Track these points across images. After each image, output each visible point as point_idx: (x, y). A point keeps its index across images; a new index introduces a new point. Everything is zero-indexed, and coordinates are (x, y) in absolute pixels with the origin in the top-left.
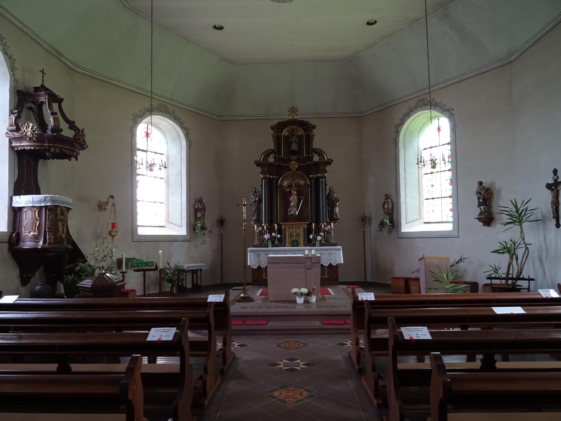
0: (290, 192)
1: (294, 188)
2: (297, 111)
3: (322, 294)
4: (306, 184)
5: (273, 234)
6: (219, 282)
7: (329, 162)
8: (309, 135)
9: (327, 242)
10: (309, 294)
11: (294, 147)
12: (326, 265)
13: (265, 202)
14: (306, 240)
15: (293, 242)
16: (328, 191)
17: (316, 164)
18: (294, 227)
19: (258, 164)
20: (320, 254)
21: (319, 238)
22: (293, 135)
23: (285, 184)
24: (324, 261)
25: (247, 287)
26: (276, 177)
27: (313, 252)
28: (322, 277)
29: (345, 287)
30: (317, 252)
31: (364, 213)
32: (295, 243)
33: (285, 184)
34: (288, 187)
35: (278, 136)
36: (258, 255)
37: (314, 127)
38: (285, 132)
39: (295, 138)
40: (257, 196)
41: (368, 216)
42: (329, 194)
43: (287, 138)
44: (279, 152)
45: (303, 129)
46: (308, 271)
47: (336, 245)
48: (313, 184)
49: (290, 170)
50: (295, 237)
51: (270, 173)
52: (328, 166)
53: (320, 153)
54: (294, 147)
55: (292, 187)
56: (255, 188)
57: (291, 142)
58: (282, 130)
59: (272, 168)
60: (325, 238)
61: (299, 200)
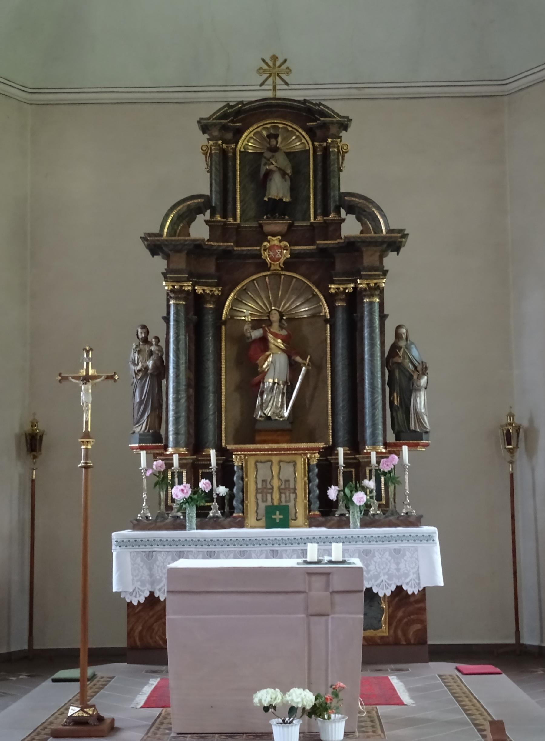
0: (264, 340)
1: (275, 328)
2: (289, 71)
3: (369, 699)
4: (315, 316)
5: (204, 484)
6: (20, 644)
7: (394, 243)
8: (326, 150)
9: (385, 513)
10: (318, 710)
11: (278, 189)
12: (384, 590)
13: (177, 376)
14: (316, 504)
15: (270, 510)
16: (390, 340)
17: (352, 246)
18: (275, 459)
19: (155, 246)
20: (365, 555)
21: (359, 498)
22: (274, 150)
23: (247, 313)
24: (376, 577)
25: (101, 670)
26: (217, 291)
27: (337, 551)
28: (371, 633)
29: (448, 668)
30: (352, 547)
31: (511, 415)
32: (278, 516)
33: (247, 313)
34: (256, 324)
35: (224, 152)
36: (149, 555)
37: (344, 125)
38: (248, 142)
39: (281, 161)
40: (151, 353)
41: (525, 423)
42: (395, 348)
43: (254, 160)
44: (226, 206)
45: (310, 132)
46: (318, 623)
47: (416, 522)
48: (340, 317)
49: (263, 266)
50: (276, 496)
51: (196, 277)
52: (392, 255)
53: (361, 208)
54: (278, 189)
55: (269, 323)
56: (144, 327)
57: (268, 174)
58: (239, 133)
59: (204, 260)
60: (379, 498)
61: (294, 369)
